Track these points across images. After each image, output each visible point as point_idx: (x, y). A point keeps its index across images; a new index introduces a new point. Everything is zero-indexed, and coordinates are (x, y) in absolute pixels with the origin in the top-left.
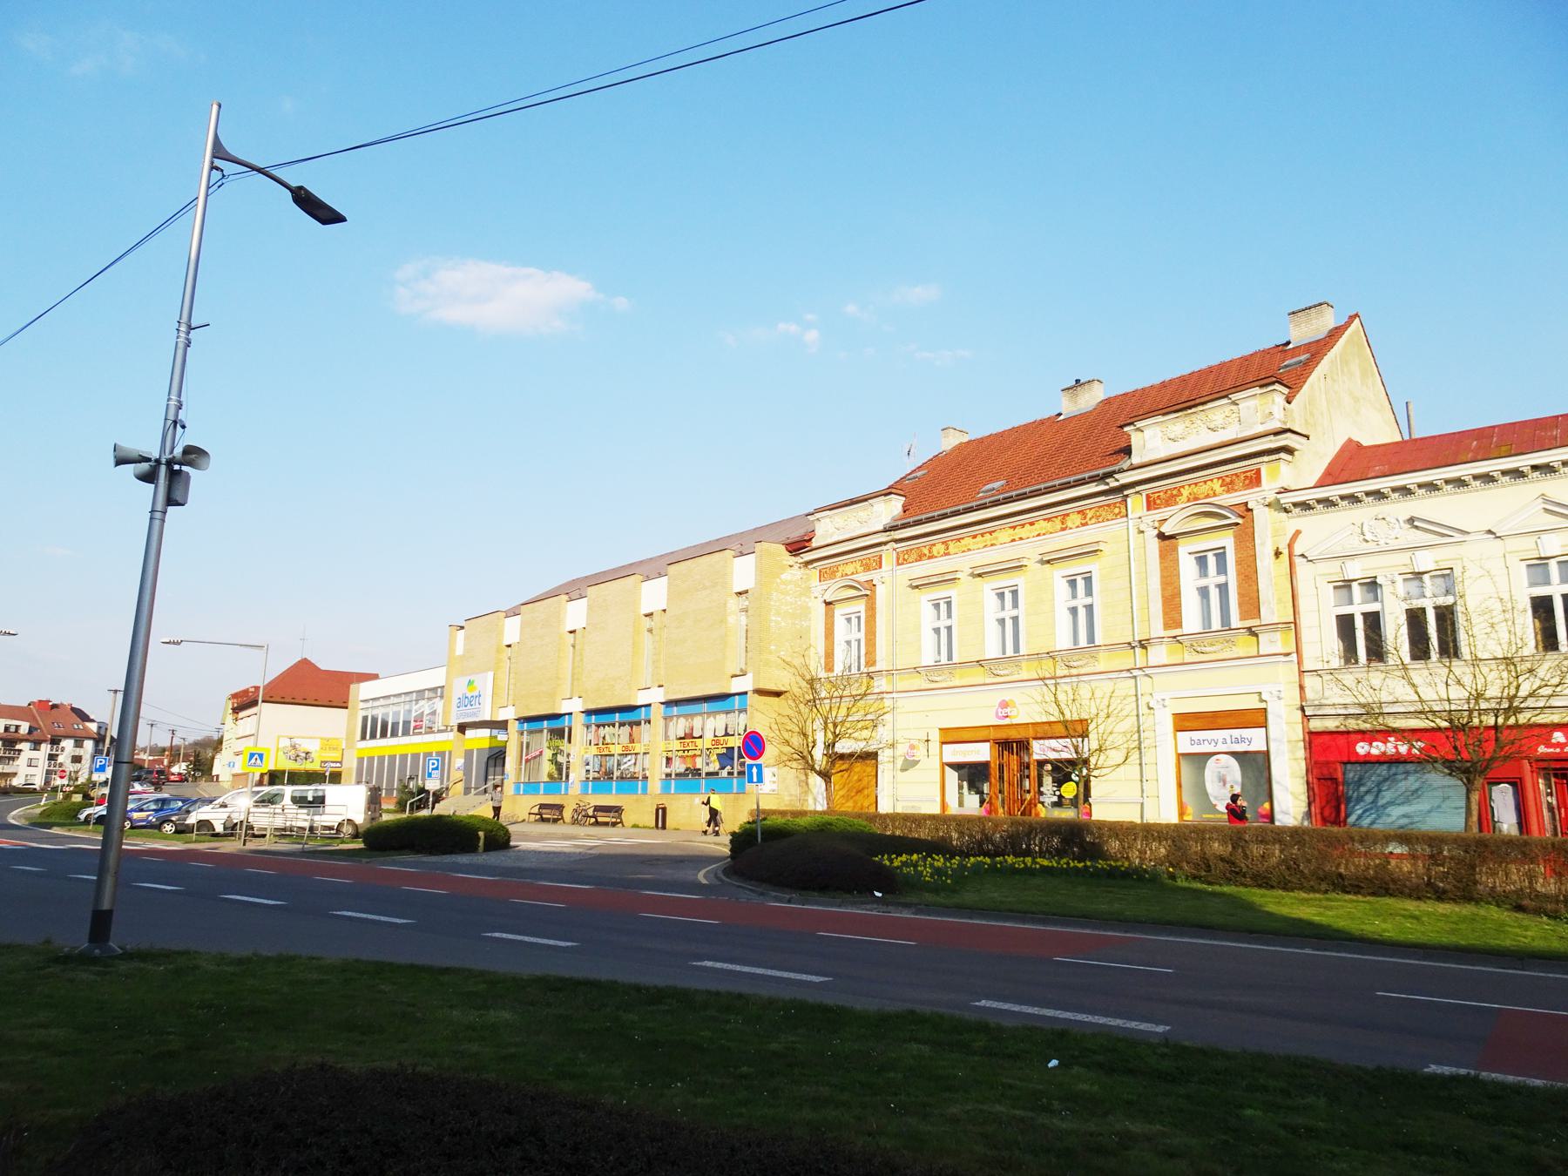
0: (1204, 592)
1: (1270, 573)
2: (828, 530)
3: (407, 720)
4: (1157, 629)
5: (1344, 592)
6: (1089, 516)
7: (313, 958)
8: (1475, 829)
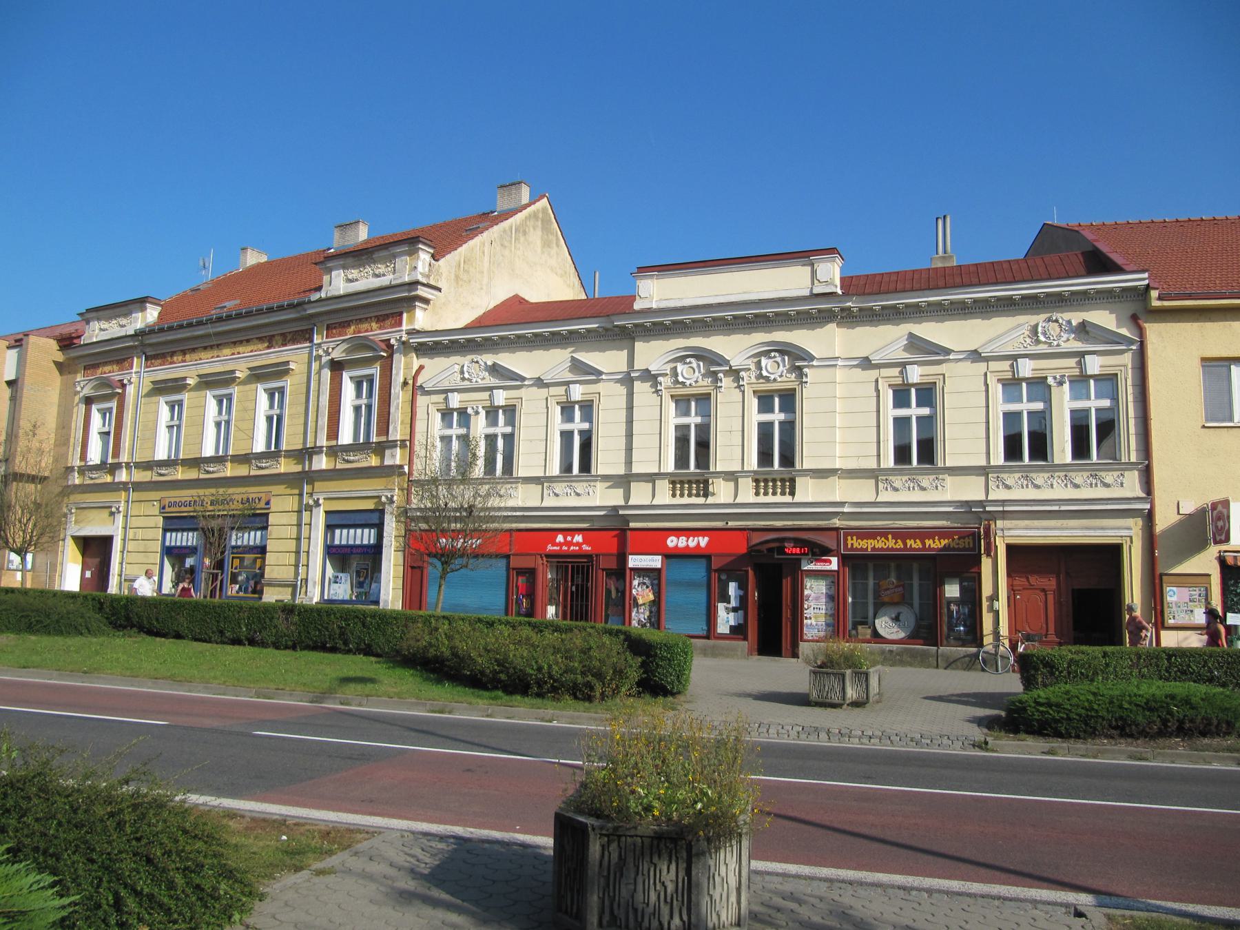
0: (357, 409)
1: (399, 397)
2: (98, 331)
3: (1013, 432)
4: (323, 441)
5: (683, 405)
6: (288, 338)
7: (85, 672)
8: (202, 597)
